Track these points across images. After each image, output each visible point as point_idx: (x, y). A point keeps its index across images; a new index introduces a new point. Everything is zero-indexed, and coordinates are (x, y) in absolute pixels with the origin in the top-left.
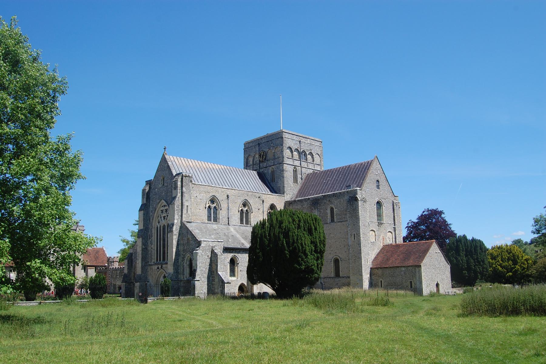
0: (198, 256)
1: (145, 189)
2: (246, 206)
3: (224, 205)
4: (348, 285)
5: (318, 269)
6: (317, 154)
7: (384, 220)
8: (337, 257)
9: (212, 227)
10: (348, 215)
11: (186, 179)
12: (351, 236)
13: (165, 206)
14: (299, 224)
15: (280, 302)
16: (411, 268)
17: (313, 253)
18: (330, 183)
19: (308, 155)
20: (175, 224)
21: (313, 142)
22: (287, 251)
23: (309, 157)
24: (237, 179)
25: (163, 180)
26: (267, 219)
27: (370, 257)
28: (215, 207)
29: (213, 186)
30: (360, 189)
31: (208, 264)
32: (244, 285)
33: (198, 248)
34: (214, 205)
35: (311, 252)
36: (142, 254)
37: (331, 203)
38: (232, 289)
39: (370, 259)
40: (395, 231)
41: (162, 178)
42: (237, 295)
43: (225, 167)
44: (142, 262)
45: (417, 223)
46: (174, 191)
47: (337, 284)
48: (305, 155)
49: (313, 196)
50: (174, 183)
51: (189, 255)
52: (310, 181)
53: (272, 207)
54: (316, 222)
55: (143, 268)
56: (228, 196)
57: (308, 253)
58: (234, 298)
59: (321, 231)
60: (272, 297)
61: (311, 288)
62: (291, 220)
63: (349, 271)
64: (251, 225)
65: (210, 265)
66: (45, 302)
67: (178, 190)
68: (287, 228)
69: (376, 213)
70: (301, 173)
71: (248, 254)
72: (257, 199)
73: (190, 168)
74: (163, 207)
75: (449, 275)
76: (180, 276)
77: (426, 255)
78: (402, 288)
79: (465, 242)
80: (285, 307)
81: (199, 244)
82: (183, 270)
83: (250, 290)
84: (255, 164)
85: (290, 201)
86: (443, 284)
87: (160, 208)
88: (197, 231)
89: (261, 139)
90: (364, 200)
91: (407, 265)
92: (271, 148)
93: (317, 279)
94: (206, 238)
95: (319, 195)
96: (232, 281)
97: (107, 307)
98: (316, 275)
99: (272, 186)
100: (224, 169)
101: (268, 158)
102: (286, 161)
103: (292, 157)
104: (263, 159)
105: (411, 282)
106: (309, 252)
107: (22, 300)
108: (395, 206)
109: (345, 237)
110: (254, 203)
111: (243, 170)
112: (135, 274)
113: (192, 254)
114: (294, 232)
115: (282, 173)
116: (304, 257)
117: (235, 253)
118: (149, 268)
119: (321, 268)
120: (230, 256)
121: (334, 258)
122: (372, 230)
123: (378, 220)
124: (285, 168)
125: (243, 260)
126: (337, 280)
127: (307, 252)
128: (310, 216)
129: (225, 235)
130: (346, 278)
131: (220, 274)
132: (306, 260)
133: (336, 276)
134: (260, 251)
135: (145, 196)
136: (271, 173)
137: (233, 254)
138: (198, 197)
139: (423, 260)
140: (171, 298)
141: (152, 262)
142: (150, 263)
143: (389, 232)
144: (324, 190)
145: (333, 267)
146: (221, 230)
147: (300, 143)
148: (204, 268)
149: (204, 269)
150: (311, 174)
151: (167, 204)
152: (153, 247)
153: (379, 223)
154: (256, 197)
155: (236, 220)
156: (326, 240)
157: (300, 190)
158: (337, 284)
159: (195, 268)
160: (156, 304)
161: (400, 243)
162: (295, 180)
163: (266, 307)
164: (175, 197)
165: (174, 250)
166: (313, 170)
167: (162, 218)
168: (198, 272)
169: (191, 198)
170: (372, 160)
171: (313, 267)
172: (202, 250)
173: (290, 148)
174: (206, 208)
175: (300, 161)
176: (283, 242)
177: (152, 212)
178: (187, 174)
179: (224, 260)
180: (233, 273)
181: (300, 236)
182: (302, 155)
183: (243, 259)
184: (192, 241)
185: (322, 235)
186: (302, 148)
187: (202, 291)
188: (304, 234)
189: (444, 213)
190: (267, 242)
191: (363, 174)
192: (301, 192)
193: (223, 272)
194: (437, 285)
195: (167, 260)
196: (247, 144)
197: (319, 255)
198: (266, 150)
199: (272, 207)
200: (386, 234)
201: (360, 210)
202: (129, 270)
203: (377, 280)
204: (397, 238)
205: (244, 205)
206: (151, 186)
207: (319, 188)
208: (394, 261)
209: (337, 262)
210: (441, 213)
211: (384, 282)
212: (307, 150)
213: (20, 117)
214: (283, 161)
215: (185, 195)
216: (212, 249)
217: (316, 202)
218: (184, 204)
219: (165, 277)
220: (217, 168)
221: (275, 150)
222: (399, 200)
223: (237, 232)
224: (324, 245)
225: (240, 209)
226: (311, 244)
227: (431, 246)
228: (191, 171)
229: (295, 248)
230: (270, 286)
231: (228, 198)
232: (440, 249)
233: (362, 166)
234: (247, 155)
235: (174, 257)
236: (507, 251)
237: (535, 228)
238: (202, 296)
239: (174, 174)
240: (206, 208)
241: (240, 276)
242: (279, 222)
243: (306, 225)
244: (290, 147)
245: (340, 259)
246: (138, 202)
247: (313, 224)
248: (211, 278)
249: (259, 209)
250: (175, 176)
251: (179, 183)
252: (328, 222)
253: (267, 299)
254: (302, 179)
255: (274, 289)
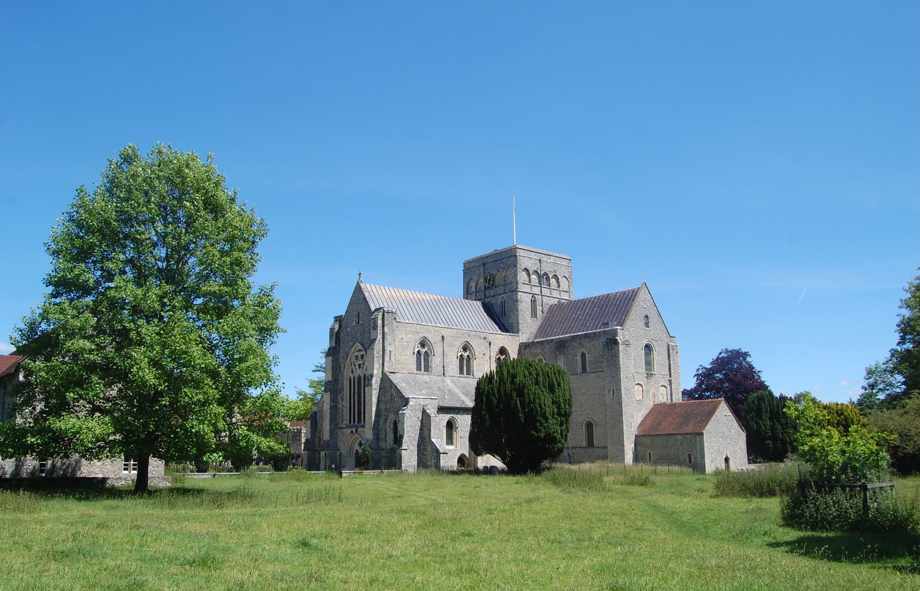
0: (405, 418)
1: (334, 328)
2: (467, 350)
3: (438, 350)
4: (605, 457)
5: (562, 437)
6: (564, 276)
7: (655, 370)
8: (590, 420)
9: (423, 379)
10: (605, 363)
11: (389, 316)
12: (609, 391)
13: (360, 350)
14: (537, 378)
15: (512, 479)
16: (690, 436)
17: (556, 416)
18: (581, 319)
19: (552, 278)
20: (374, 375)
21: (559, 261)
22: (522, 414)
23: (553, 281)
24: (455, 313)
25: (357, 317)
26: (495, 370)
27: (635, 420)
28: (426, 352)
29: (423, 324)
30: (622, 328)
31: (419, 429)
32: (465, 456)
33: (405, 408)
34: (424, 350)
35: (553, 415)
36: (330, 413)
37: (583, 347)
38: (449, 461)
39: (635, 423)
40: (671, 384)
41: (356, 313)
42: (455, 468)
43: (439, 297)
44: (330, 424)
45: (711, 369)
46: (372, 331)
47: (590, 456)
48: (548, 279)
49: (558, 337)
50: (372, 321)
51: (393, 416)
52: (553, 315)
53: (503, 351)
54: (559, 375)
55: (332, 432)
56: (443, 337)
57: (549, 416)
58: (453, 473)
59: (566, 388)
60: (502, 472)
61: (553, 461)
62: (527, 373)
63: (607, 439)
64: (473, 375)
65: (420, 429)
66: (220, 474)
67: (379, 331)
68: (521, 384)
69: (644, 361)
70: (542, 304)
71: (471, 416)
72: (482, 341)
73: (393, 301)
74: (357, 351)
75: (744, 446)
76: (381, 443)
77: (710, 418)
78: (676, 464)
79: (769, 400)
80: (518, 485)
81: (406, 401)
82: (386, 435)
83: (473, 463)
84: (479, 292)
85: (526, 343)
86: (735, 458)
87: (353, 353)
88: (404, 385)
89: (487, 257)
90: (627, 343)
91: (684, 432)
92: (501, 270)
93: (561, 450)
94: (415, 394)
95: (565, 336)
96: (449, 450)
97: (302, 481)
98: (560, 445)
99: (502, 321)
100: (437, 300)
101: (496, 283)
102: (521, 287)
103: (530, 282)
104: (489, 284)
105: (690, 455)
106: (550, 414)
107: (192, 471)
108: (671, 351)
109: (601, 393)
110: (478, 347)
111: (463, 300)
112: (320, 439)
113: (398, 414)
114: (530, 389)
115: (515, 304)
116: (543, 421)
117: (453, 413)
118: (339, 434)
119: (566, 436)
120: (446, 417)
121: (586, 422)
122: (638, 384)
123: (646, 369)
124: (519, 297)
125: (463, 422)
126: (590, 450)
127: (548, 414)
128: (551, 368)
129: (440, 389)
130: (602, 448)
131: (434, 442)
132: (546, 425)
133: (589, 445)
134: (487, 413)
135: (334, 337)
136: (501, 303)
137: (451, 415)
138: (404, 339)
139: (706, 426)
140: (371, 472)
141: (344, 424)
142: (340, 426)
143: (662, 386)
144: (573, 328)
145: (584, 433)
146: (435, 383)
147: (540, 263)
148: (413, 433)
149: (413, 435)
150: (555, 305)
151: (364, 348)
152: (344, 404)
153: (647, 374)
154: (481, 338)
155: (453, 369)
156: (573, 400)
157: (540, 327)
158: (590, 456)
159: (402, 433)
160: (354, 479)
161: (677, 401)
162: (534, 314)
163: (495, 484)
164: (375, 339)
165: (374, 409)
166: (558, 300)
167: (357, 367)
168: (405, 439)
169: (395, 341)
170: (639, 288)
171: (555, 434)
172: (410, 410)
173: (526, 270)
174: (414, 353)
175: (541, 287)
176: (516, 402)
177: (342, 358)
178: (390, 310)
179: (439, 422)
180: (450, 440)
181: (538, 394)
182: (544, 278)
183: (464, 422)
184: (397, 397)
185: (567, 393)
186: (543, 269)
187: (410, 463)
188: (542, 391)
189: (750, 356)
190: (495, 402)
191: (626, 307)
192: (541, 331)
193: (438, 438)
194: (727, 460)
195: (364, 421)
196: (468, 264)
197: (563, 419)
198: (494, 272)
199: (503, 351)
200: (658, 389)
201: (621, 357)
202: (312, 434)
203: (644, 451)
204: (673, 395)
205: (465, 349)
206: (342, 324)
207: (567, 324)
208: (667, 427)
209: (589, 426)
210: (746, 355)
211: (654, 455)
212: (550, 271)
213: (226, 272)
214: (517, 289)
215: (387, 336)
216: (423, 408)
217: (561, 346)
218: (386, 348)
219: (360, 444)
220: (428, 298)
221: (506, 273)
222: (678, 342)
223: (456, 385)
224: (570, 406)
225: (460, 354)
226: (553, 404)
227: (718, 406)
228: (394, 304)
229: (531, 410)
230: (499, 458)
231: (443, 339)
232: (731, 411)
233: (625, 296)
234: (468, 279)
235: (373, 418)
236: (837, 412)
237: (867, 381)
238: (411, 470)
239: (373, 309)
240: (414, 353)
241: (460, 444)
242: (511, 375)
243: (546, 379)
244: (526, 269)
245: (594, 423)
246: (325, 343)
247: (556, 378)
248: (422, 446)
249: (484, 355)
250: (374, 312)
251: (380, 322)
252: (579, 373)
253: (495, 474)
254: (543, 312)
255: (504, 463)
